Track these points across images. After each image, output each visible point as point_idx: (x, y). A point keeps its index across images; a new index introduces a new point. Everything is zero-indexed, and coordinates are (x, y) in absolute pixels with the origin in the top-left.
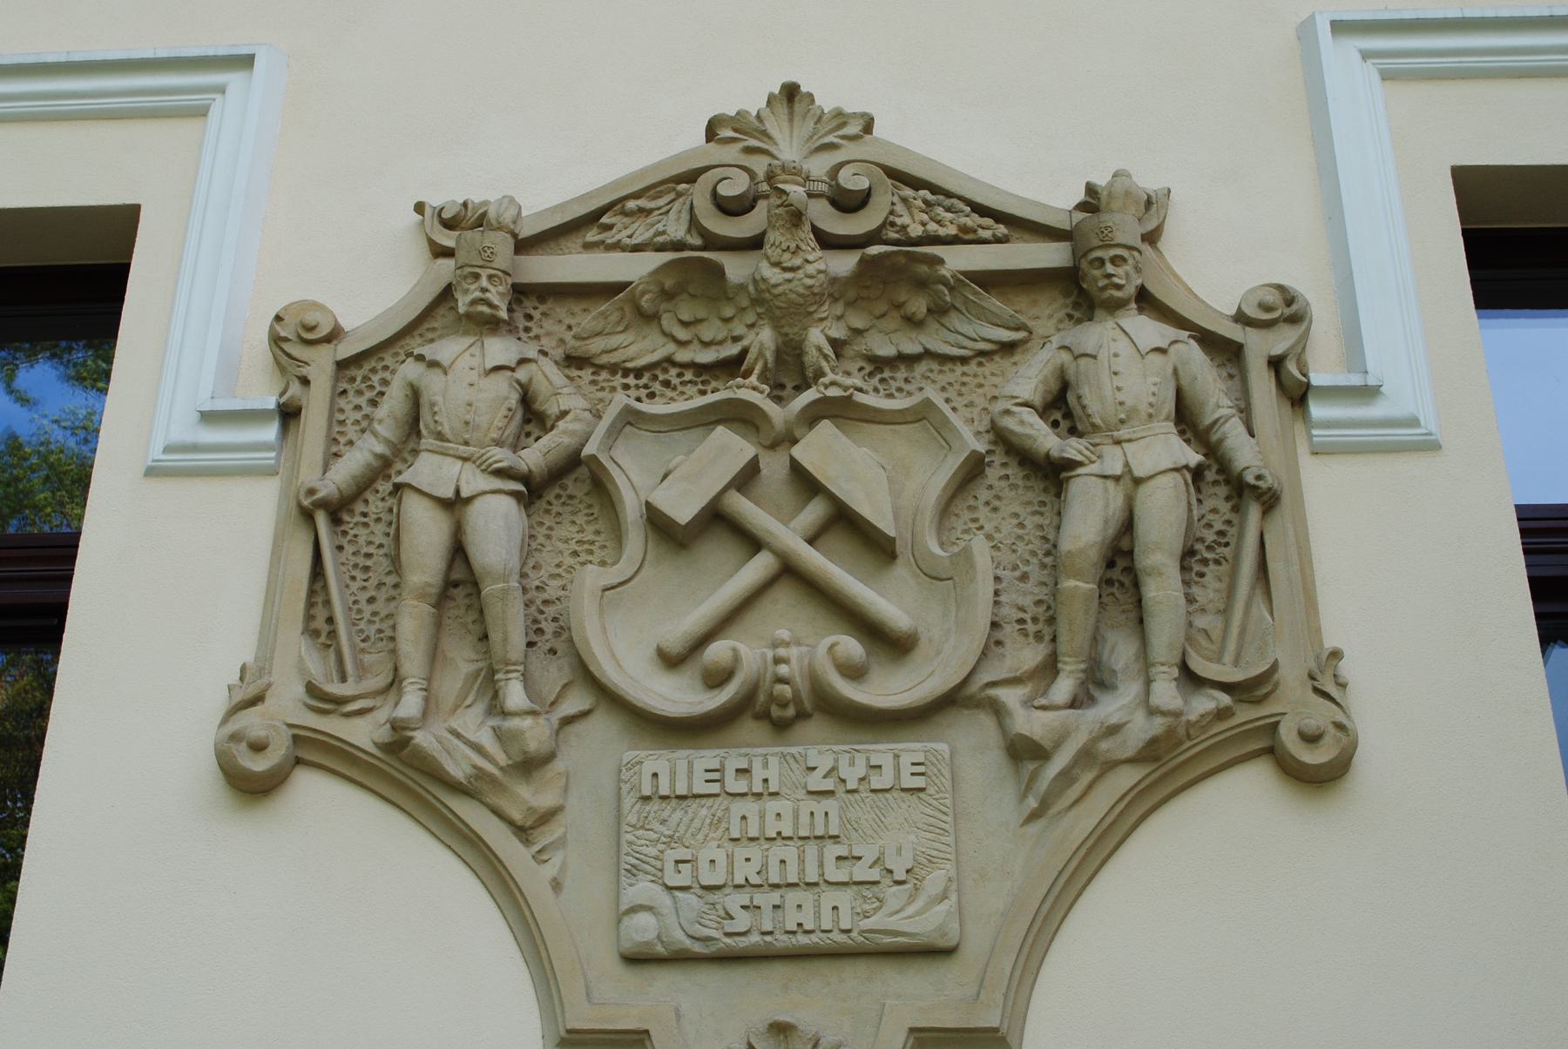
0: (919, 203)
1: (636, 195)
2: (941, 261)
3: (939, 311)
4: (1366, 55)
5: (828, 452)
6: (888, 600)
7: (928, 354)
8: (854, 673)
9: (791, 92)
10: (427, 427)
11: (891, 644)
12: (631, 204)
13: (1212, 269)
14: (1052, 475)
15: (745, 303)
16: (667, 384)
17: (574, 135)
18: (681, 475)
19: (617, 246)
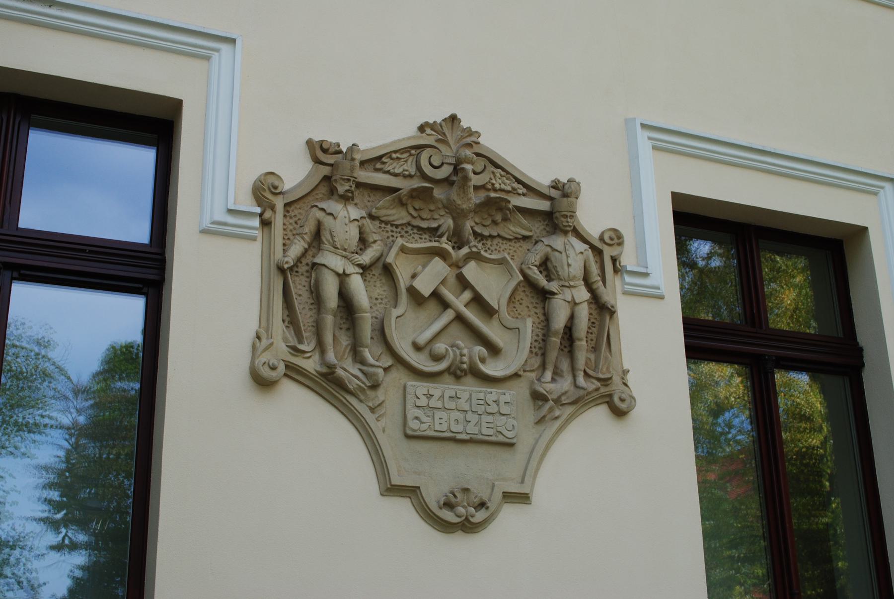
0: (498, 175)
1: (395, 152)
2: (509, 202)
3: (505, 219)
4: (649, 138)
5: (471, 271)
6: (491, 330)
7: (499, 236)
8: (483, 361)
9: (453, 119)
10: (327, 240)
11: (494, 350)
12: (394, 156)
13: (592, 216)
14: (545, 295)
15: (440, 206)
16: (407, 232)
17: (376, 126)
18: (431, 276)
19: (388, 172)
